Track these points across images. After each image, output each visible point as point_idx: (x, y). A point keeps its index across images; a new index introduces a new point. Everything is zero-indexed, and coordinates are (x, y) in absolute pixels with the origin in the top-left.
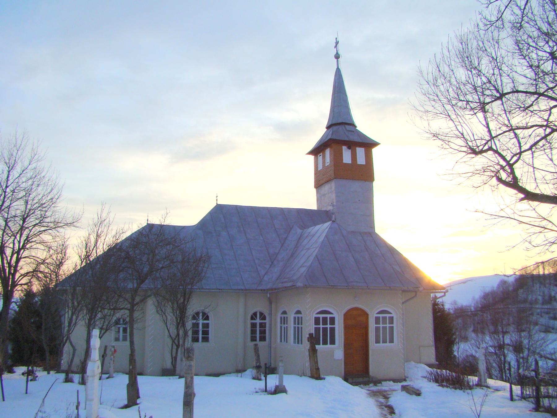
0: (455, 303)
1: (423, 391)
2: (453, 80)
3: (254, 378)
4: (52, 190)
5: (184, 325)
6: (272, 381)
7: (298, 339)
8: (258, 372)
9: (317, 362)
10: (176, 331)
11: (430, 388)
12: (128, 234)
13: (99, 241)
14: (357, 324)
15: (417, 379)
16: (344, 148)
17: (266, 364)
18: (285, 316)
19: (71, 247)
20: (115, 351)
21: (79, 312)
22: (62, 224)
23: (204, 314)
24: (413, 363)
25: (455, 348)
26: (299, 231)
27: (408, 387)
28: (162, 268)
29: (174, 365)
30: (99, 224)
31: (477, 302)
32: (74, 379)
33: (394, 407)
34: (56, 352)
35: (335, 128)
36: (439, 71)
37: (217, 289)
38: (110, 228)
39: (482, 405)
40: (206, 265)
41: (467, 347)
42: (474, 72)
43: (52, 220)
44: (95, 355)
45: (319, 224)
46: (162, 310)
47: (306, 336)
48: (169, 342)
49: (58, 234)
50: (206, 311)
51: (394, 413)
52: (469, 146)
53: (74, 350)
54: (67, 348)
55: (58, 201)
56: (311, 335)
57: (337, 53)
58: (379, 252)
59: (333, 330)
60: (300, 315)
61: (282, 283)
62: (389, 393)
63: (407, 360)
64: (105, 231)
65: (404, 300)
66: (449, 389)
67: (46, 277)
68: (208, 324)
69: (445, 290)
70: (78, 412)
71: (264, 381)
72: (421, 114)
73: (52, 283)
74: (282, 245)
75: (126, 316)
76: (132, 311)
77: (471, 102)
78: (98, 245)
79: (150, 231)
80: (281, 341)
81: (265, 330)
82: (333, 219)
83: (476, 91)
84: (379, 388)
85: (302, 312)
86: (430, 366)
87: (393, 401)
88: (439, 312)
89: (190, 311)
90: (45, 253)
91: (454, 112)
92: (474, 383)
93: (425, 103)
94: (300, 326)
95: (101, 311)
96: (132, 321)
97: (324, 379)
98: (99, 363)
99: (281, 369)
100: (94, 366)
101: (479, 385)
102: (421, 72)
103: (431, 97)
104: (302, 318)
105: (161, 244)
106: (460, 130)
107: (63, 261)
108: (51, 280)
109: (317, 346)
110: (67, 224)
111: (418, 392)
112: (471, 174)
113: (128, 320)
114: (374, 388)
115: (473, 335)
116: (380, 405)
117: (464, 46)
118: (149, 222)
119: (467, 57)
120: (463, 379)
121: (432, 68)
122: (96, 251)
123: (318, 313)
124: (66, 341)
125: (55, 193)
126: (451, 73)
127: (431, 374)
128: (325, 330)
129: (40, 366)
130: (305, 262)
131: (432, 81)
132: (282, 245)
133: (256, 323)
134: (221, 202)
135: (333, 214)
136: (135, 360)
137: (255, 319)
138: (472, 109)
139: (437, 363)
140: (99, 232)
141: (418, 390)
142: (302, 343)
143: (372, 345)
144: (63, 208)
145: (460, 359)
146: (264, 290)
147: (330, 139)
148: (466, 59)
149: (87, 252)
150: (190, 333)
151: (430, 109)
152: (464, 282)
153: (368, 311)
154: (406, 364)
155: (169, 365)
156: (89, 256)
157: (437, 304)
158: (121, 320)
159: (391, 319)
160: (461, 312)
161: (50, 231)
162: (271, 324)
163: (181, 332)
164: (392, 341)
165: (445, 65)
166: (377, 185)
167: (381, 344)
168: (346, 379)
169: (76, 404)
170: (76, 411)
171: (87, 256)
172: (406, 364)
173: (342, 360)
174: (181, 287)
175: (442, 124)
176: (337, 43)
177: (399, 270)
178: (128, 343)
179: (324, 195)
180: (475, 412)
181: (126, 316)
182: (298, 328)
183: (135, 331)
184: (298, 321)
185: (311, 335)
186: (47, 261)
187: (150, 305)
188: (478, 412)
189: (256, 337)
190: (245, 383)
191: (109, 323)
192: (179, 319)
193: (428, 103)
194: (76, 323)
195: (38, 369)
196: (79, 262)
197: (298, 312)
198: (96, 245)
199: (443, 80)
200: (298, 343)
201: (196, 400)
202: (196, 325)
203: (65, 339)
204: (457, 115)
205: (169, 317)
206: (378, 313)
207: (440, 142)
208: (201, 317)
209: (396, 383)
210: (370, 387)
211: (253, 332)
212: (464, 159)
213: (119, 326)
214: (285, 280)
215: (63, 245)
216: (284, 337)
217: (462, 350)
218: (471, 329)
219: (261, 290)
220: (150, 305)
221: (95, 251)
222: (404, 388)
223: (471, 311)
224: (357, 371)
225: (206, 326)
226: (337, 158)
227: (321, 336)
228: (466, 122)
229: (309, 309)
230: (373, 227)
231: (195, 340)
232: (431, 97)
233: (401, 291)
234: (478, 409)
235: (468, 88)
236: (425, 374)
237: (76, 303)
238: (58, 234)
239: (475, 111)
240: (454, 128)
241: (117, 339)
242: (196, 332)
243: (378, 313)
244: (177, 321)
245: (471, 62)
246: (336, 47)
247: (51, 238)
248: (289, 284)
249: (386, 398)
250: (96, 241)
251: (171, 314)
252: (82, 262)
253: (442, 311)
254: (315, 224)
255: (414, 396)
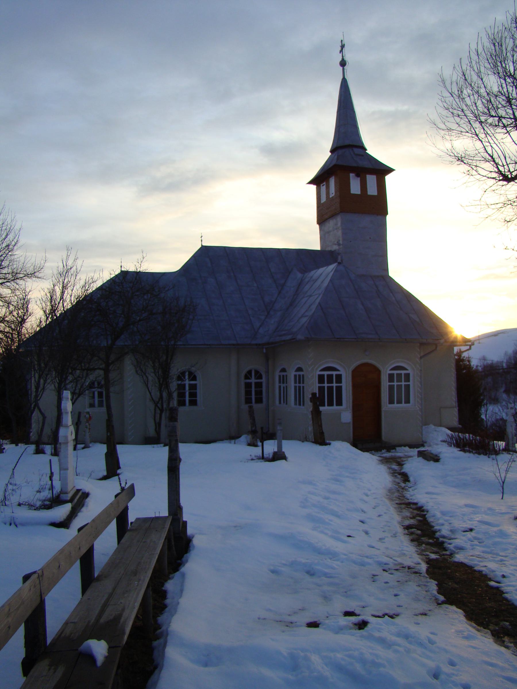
0: (484, 359)
1: (441, 456)
2: (482, 91)
3: (249, 445)
4: (7, 235)
5: (167, 386)
6: (270, 447)
7: (299, 400)
8: (253, 438)
9: (321, 426)
10: (158, 394)
11: (449, 453)
12: (99, 284)
13: (66, 292)
14: (367, 382)
15: (437, 444)
16: (352, 175)
17: (262, 428)
18: (284, 374)
19: (34, 302)
20: (90, 418)
21: (47, 375)
22: (22, 276)
23: (190, 373)
24: (433, 427)
25: (483, 410)
26: (299, 275)
27: (426, 452)
28: (140, 320)
29: (158, 431)
30: (64, 273)
31: (510, 358)
32: (45, 450)
33: (409, 474)
34: (25, 422)
35: (340, 152)
36: (466, 80)
37: (205, 345)
38: (78, 278)
39: (507, 471)
40: (191, 317)
41: (497, 410)
42: (508, 80)
43: (10, 271)
44: (68, 419)
45: (322, 267)
46: (142, 371)
47: (308, 396)
48: (152, 406)
49: (17, 287)
50: (193, 369)
51: (409, 481)
52: (500, 171)
53: (44, 418)
54: (36, 416)
55: (16, 248)
56: (314, 394)
57: (343, 59)
58: (394, 298)
59: (339, 389)
60: (301, 373)
61: (281, 336)
62: (404, 459)
63: (426, 424)
64: (72, 280)
65: (422, 354)
66: (471, 455)
67: (7, 337)
68: (196, 385)
69: (469, 343)
70: (52, 483)
71: (260, 448)
72: (443, 132)
73: (14, 344)
74: (280, 292)
75: (100, 378)
76: (107, 371)
77: (504, 118)
78: (65, 298)
79: (124, 278)
80: (280, 403)
81: (261, 391)
82: (339, 260)
83: (511, 105)
84: (393, 454)
85: (304, 370)
86: (451, 429)
87: (407, 468)
88: (464, 369)
89: (175, 370)
90: (4, 310)
91: (482, 130)
92: (501, 448)
93: (448, 119)
94: (301, 385)
95: (71, 373)
96: (107, 384)
97: (330, 444)
98: (72, 429)
99: (279, 434)
100: (68, 433)
101: (507, 450)
102: (443, 81)
103: (455, 112)
104: (303, 375)
105: (137, 294)
106: (490, 152)
107: (25, 317)
108: (12, 340)
109: (321, 408)
110: (27, 275)
111: (436, 458)
112: (500, 205)
113: (103, 382)
114: (388, 455)
115: (504, 396)
116: (393, 473)
117: (497, 48)
118: (123, 269)
119: (501, 62)
120: (489, 442)
121: (457, 76)
122: (63, 305)
123: (321, 370)
124: (34, 408)
125: (11, 239)
126: (480, 82)
127: (452, 438)
128: (330, 389)
129: (6, 439)
130: (306, 311)
131: (456, 93)
132: (280, 292)
133: (251, 383)
134: (206, 244)
135: (339, 254)
136: (113, 426)
137: (250, 379)
138: (505, 126)
139: (460, 426)
140: (65, 282)
141: (436, 456)
142: (303, 405)
143: (386, 406)
144: (22, 257)
145: (489, 423)
146: (260, 344)
147: (335, 166)
148: (499, 64)
149: (52, 306)
150: (175, 395)
151: (454, 126)
152: (496, 334)
153: (381, 368)
154: (424, 427)
155: (152, 432)
156: (55, 310)
157: (463, 360)
158: (96, 384)
159: (407, 376)
160: (491, 370)
161: (8, 284)
162: (268, 384)
163: (165, 394)
164: (408, 401)
165: (472, 73)
166: (390, 219)
167: (396, 405)
168: (355, 444)
169: (49, 475)
170: (50, 482)
171: (53, 310)
172: (424, 427)
173: (349, 423)
174: (162, 343)
175: (465, 144)
176: (343, 47)
177: (418, 320)
178: (104, 409)
179: (329, 232)
180: (499, 478)
181: (100, 378)
182: (300, 387)
183: (111, 394)
184: (299, 379)
185: (314, 394)
186: (7, 319)
187: (128, 365)
188: (503, 479)
189: (251, 399)
190: (240, 450)
191: (82, 386)
192: (161, 380)
193: (451, 119)
194: (44, 389)
195: (5, 441)
196: (44, 318)
197: (299, 369)
198: (62, 298)
199: (469, 91)
200: (300, 404)
201: (183, 468)
202: (181, 387)
203: (33, 406)
204: (486, 134)
205: (150, 378)
206: (391, 370)
207: (467, 168)
208: (187, 377)
209: (412, 449)
210: (382, 454)
211: (248, 393)
212: (493, 188)
213: (93, 390)
214: (284, 332)
215: (24, 299)
216: (284, 398)
217: (490, 412)
218: (502, 390)
219: (256, 345)
220: (128, 365)
221: (61, 305)
222: (421, 454)
223: (503, 369)
224: (368, 436)
225: (193, 387)
226: (344, 187)
227: (327, 395)
228: (496, 142)
229: (311, 367)
230: (387, 270)
231: (182, 403)
232: (455, 112)
233: (419, 344)
234: (503, 475)
235: (501, 100)
236: (444, 438)
237: (43, 365)
238: (17, 287)
239: (508, 129)
240: (482, 150)
241: (92, 405)
242: (181, 395)
243: (391, 370)
244: (159, 381)
245: (505, 68)
246: (341, 51)
247: (10, 292)
248: (289, 337)
249: (400, 464)
250: (63, 293)
251: (153, 375)
252: (47, 318)
253: (469, 367)
254: (318, 268)
255: (432, 462)
